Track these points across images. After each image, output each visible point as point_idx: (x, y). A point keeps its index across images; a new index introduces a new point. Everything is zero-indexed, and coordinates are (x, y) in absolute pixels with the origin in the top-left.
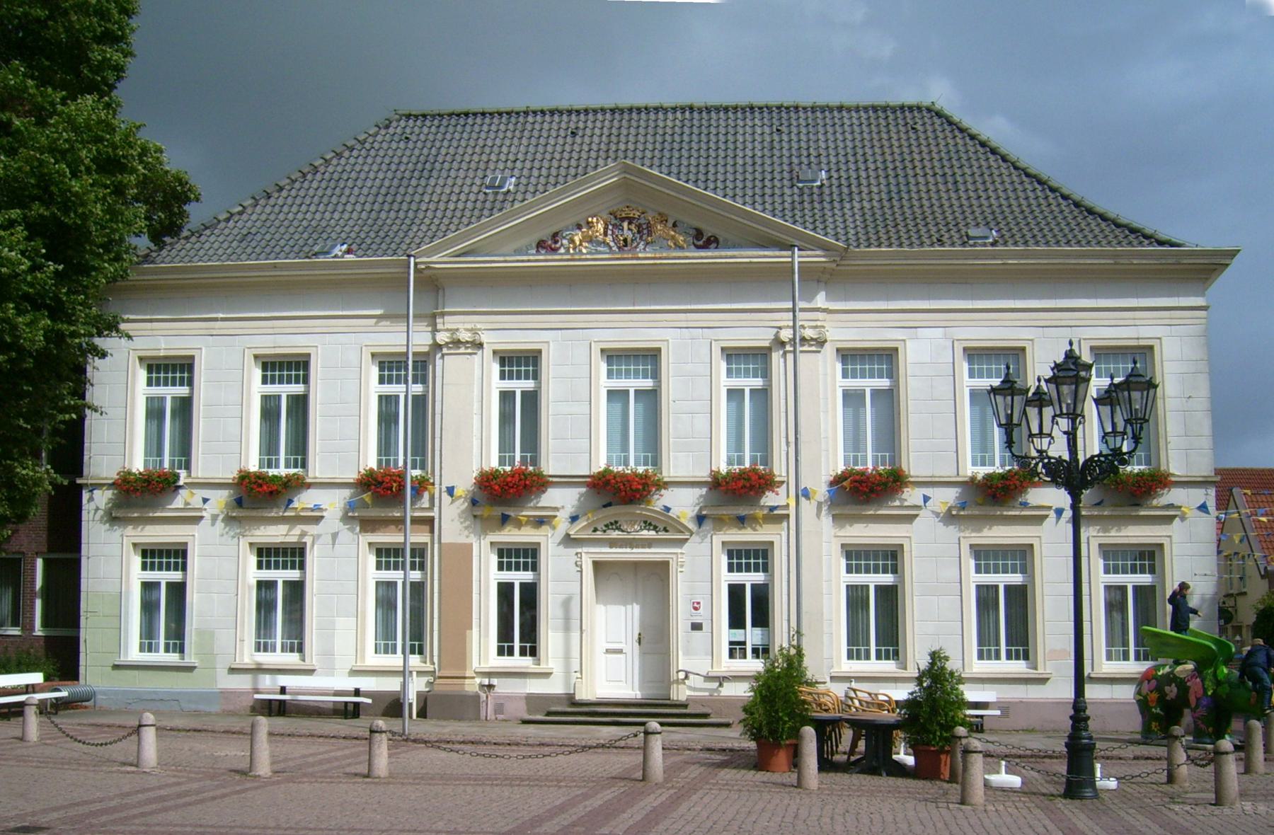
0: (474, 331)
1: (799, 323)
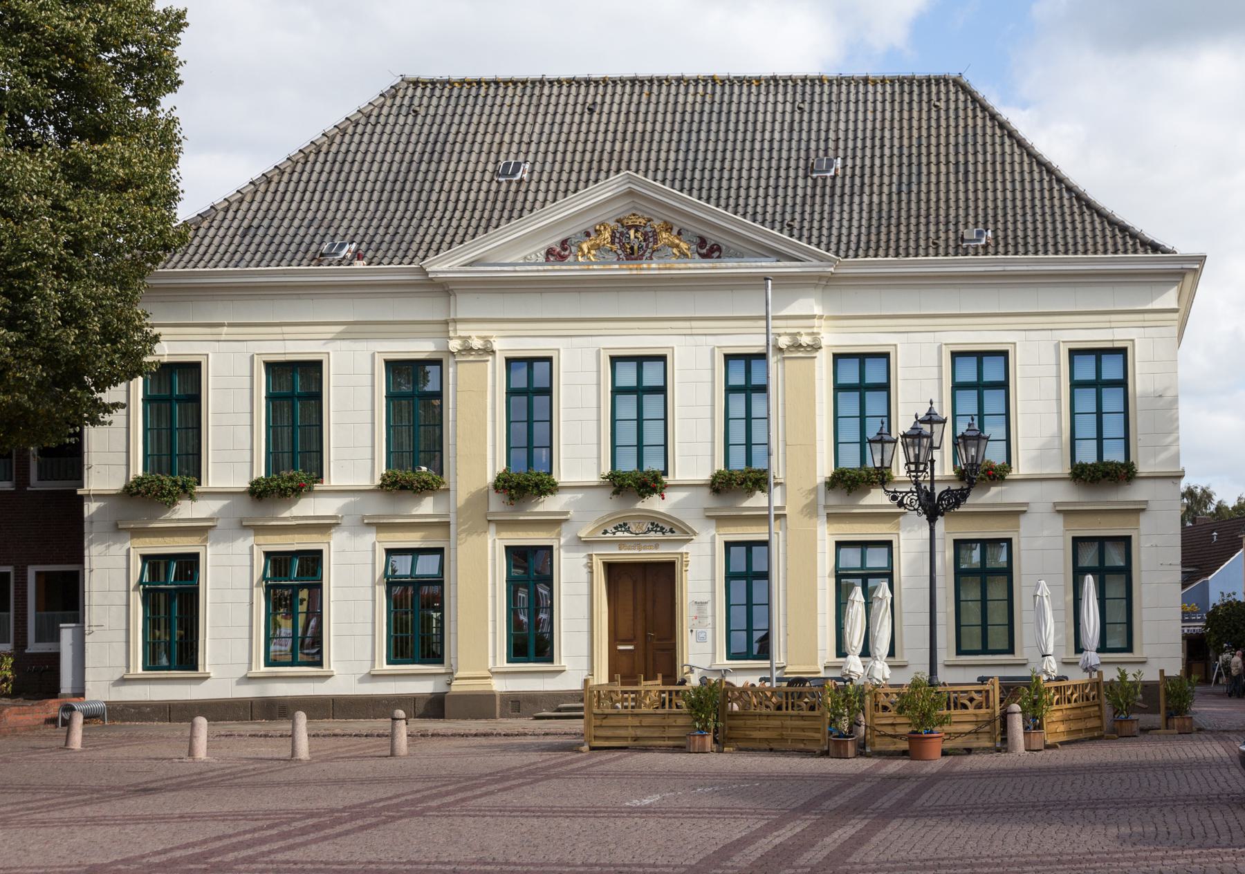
0: (486, 340)
1: (771, 331)
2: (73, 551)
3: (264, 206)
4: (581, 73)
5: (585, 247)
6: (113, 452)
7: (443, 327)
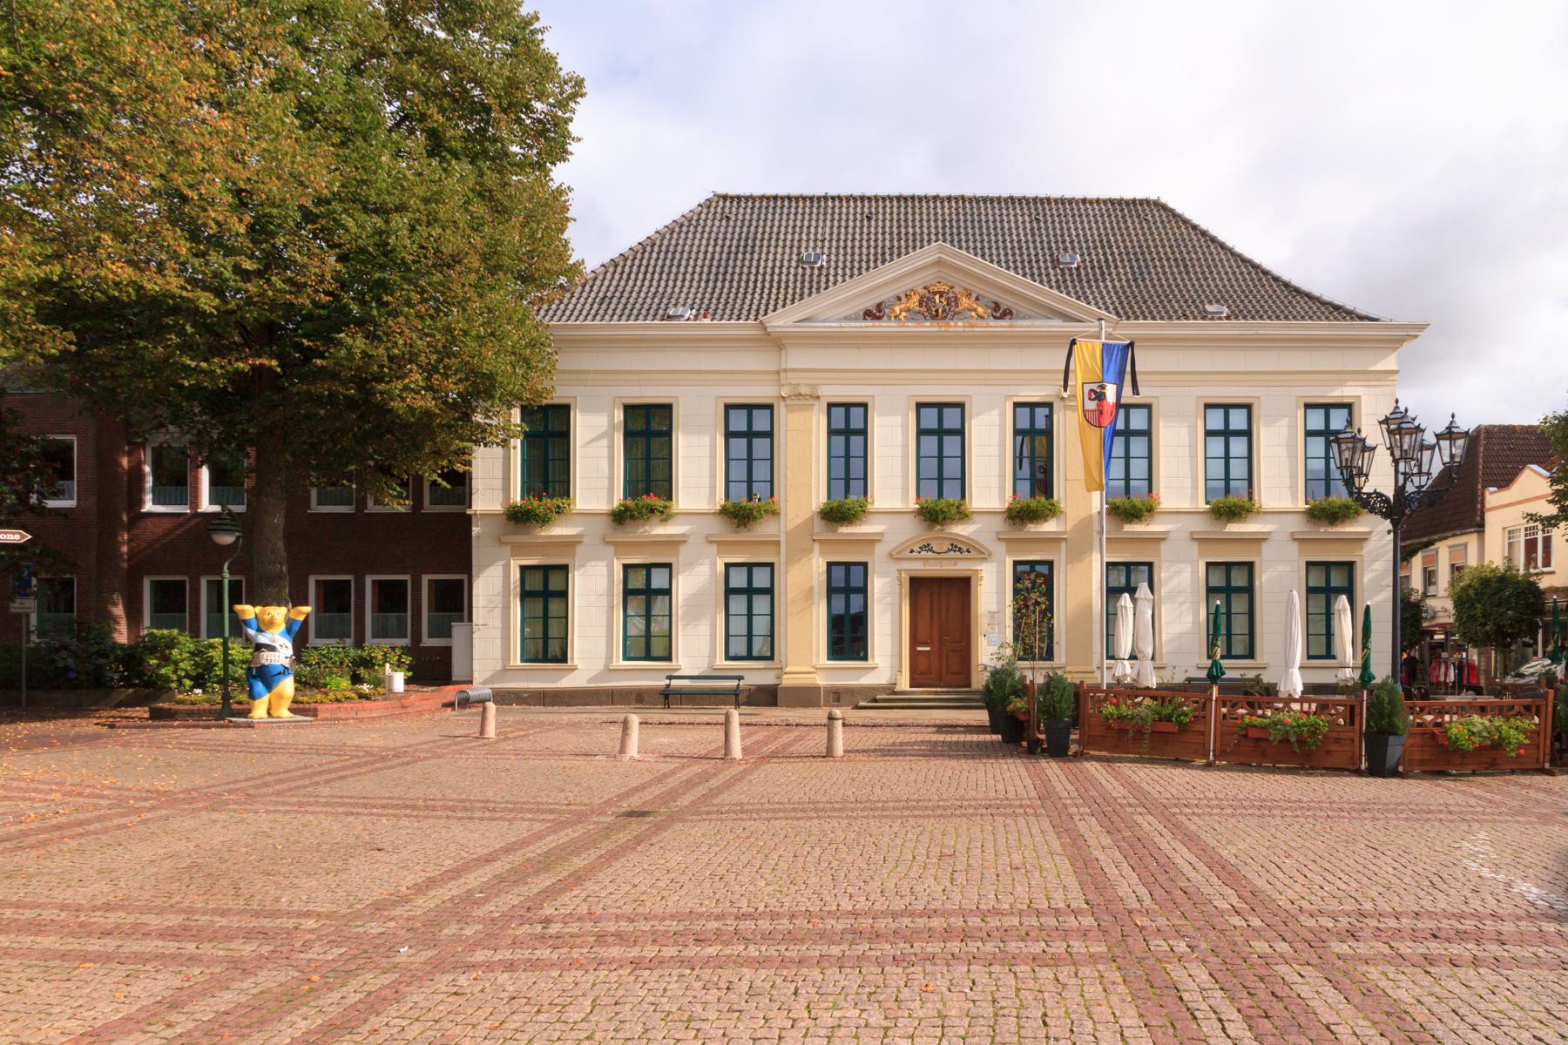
2: (463, 562)
3: (614, 283)
4: (857, 192)
5: (897, 309)
6: (495, 476)
7: (774, 377)
